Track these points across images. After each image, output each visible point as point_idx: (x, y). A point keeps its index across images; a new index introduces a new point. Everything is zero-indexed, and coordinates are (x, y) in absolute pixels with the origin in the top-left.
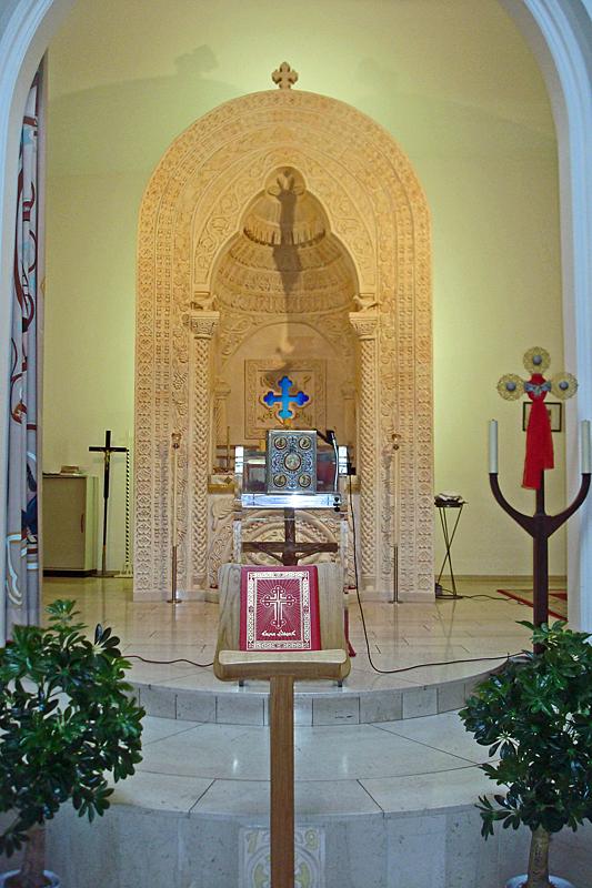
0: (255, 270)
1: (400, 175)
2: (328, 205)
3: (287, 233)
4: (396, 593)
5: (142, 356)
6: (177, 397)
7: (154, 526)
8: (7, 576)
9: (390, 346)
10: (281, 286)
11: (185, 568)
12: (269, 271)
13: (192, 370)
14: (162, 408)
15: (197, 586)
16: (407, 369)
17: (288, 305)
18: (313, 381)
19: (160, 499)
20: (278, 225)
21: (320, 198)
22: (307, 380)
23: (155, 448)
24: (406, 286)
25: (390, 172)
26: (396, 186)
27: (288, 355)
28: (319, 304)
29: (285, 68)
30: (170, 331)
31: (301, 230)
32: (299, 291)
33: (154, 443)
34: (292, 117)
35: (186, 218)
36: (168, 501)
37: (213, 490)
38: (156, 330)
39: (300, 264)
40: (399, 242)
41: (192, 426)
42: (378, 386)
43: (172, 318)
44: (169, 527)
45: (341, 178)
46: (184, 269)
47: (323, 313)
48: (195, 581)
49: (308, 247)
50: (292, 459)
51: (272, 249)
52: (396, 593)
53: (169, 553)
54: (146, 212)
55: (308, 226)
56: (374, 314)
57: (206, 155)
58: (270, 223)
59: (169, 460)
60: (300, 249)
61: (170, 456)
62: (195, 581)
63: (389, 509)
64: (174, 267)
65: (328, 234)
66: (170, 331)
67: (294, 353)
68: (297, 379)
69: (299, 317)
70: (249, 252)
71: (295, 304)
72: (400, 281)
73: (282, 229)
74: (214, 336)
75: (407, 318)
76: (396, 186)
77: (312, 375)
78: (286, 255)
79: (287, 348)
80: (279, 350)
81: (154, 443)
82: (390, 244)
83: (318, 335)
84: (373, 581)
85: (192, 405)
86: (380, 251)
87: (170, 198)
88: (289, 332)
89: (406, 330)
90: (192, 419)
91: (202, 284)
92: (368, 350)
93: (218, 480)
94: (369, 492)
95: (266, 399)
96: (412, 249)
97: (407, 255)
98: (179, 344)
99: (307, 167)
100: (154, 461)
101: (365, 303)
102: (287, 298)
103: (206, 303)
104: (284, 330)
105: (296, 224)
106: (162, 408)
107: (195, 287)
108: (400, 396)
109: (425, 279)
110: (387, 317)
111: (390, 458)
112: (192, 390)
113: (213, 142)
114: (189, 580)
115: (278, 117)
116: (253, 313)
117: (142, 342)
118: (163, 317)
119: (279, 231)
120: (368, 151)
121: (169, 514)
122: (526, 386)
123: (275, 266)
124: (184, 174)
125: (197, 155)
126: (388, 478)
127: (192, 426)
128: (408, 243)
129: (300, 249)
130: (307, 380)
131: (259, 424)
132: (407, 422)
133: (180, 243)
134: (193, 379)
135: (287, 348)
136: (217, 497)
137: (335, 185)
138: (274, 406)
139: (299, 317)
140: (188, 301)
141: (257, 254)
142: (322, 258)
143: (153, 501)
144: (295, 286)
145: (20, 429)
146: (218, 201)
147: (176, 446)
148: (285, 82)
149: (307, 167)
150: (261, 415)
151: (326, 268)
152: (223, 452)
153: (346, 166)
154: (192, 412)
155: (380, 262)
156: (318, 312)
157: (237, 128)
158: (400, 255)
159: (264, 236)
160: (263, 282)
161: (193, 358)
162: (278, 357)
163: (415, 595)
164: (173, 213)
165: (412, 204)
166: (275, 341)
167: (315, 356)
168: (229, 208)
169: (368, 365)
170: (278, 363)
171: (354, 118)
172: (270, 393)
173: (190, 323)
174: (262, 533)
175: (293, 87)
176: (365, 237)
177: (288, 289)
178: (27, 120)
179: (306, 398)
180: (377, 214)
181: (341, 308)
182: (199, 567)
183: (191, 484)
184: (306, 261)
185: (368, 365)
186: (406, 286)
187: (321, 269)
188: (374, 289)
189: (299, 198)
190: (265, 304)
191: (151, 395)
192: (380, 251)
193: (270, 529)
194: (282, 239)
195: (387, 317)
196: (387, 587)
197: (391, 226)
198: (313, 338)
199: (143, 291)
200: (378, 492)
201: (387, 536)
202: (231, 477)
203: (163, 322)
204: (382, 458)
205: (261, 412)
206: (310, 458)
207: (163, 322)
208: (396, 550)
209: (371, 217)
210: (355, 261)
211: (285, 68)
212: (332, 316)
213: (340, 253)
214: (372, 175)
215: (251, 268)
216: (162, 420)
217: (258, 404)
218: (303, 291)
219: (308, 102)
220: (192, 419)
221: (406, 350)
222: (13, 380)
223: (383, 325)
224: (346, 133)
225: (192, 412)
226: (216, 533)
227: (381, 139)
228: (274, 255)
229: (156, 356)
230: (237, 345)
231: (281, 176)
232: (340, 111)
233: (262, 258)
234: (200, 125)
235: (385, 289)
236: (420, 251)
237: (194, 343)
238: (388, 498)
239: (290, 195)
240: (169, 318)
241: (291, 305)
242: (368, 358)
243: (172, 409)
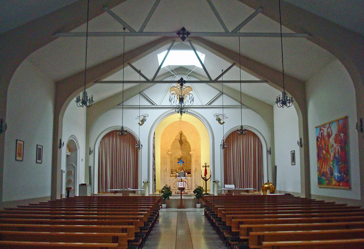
5: (161, 158)
8: (153, 186)
29: (182, 78)
31: (183, 138)
32: (183, 146)
37: (171, 176)
50: (182, 174)
68: (183, 159)
74: (171, 155)
78: (181, 142)
80: (180, 155)
91: (169, 148)
93: (171, 175)
100: (163, 173)
103: (170, 151)
104: (180, 152)
107: (168, 148)
109: (200, 147)
112: (168, 163)
117: (161, 156)
122: (205, 166)
135: (181, 155)
138: (179, 164)
145: (154, 170)
152: (172, 171)
161: (168, 158)
166: (179, 154)
170: (180, 157)
173: (167, 153)
177: (181, 146)
178: (154, 138)
179: (184, 162)
201: (195, 183)
205: (177, 164)
206: (183, 174)
211: (182, 78)
213: (187, 142)
222: (153, 166)
239: (181, 134)
243: (165, 165)
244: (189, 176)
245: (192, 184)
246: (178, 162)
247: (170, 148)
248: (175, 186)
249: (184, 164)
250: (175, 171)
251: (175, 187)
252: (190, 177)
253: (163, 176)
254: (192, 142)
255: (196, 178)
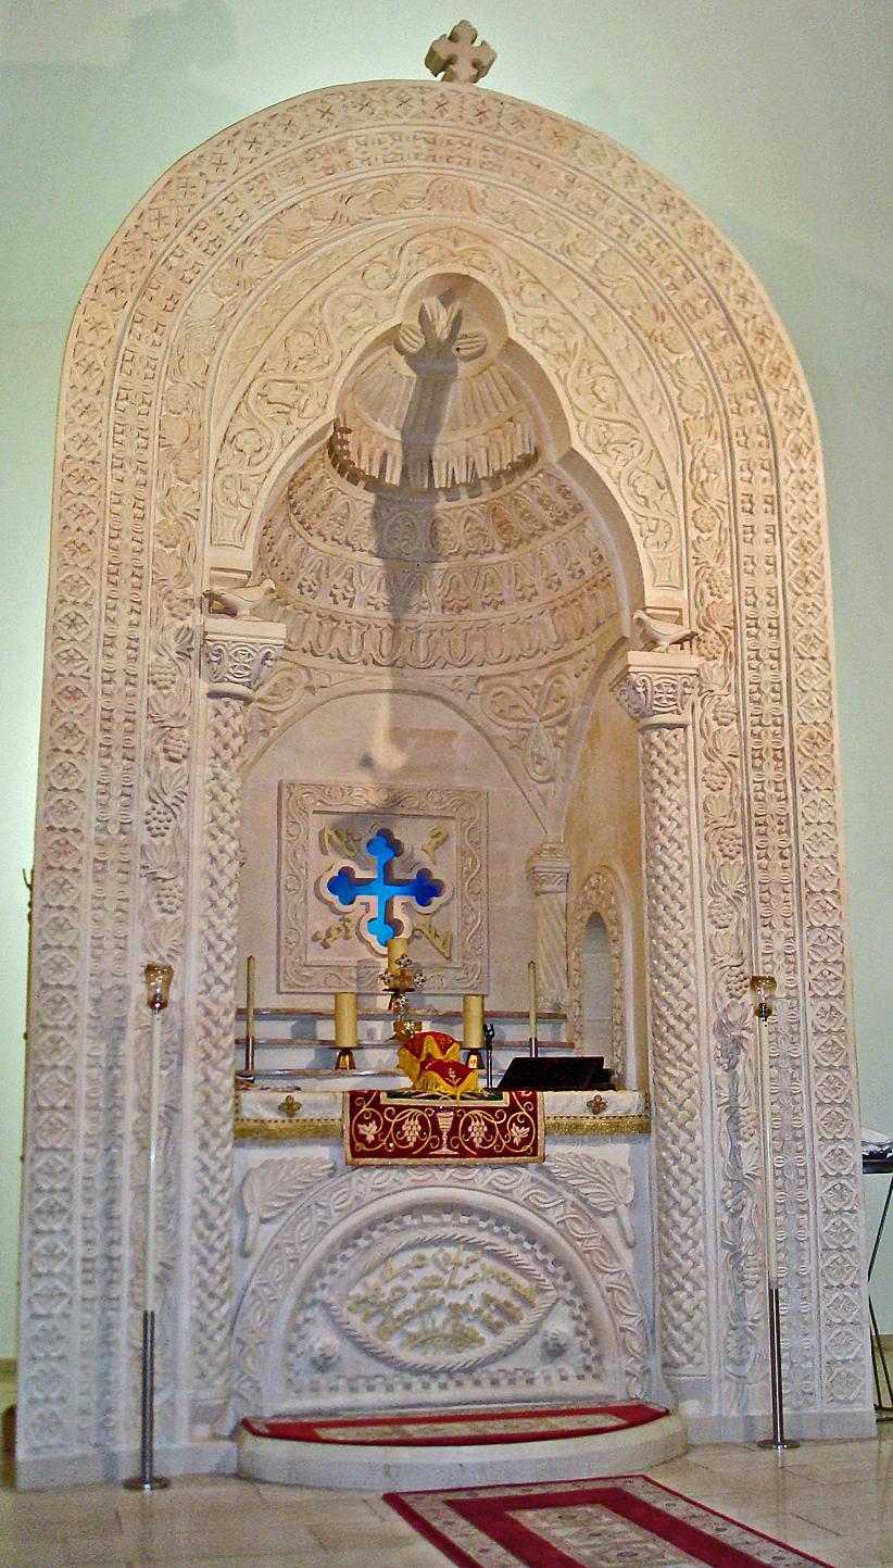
0: (323, 546)
1: (740, 325)
2: (564, 382)
3: (419, 458)
4: (777, 1417)
6: (156, 861)
7: (80, 1249)
9: (727, 744)
10: (382, 597)
11: (172, 1376)
12: (357, 555)
13: (199, 785)
14: (111, 889)
15: (203, 1430)
16: (774, 806)
17: (395, 647)
18: (453, 843)
19: (99, 1167)
20: (398, 437)
21: (542, 361)
22: (441, 839)
23: (89, 1008)
24: (763, 597)
25: (715, 317)
26: (731, 352)
27: (393, 775)
28: (477, 647)
30: (141, 669)
32: (427, 612)
33: (86, 992)
34: (477, 155)
35: (194, 370)
36: (123, 1170)
37: (247, 1134)
38: (102, 663)
39: (435, 545)
40: (741, 487)
41: (195, 944)
42: (698, 851)
43: (146, 635)
44: (125, 1251)
45: (592, 319)
46: (184, 503)
47: (482, 671)
48: (200, 1414)
49: (465, 499)
51: (371, 498)
52: (777, 1417)
53: (127, 1334)
54: (89, 337)
55: (482, 440)
56: (689, 660)
57: (254, 213)
58: (379, 426)
59: (127, 1047)
60: (442, 503)
61: (132, 1033)
62: (200, 1414)
63: (738, 1181)
64: (157, 494)
65: (552, 454)
66: (141, 669)
67: (408, 770)
69: (412, 678)
70: (491, 408)
71: (414, 643)
72: (746, 579)
73: (406, 446)
75: (767, 675)
76: (731, 352)
77: (452, 826)
79: (388, 756)
80: (367, 762)
81: (86, 992)
82: (717, 491)
83: (463, 726)
84: (700, 1389)
85: (198, 884)
86: (692, 506)
87: (153, 310)
88: (396, 716)
89: (768, 707)
90: (197, 924)
92: (668, 752)
94: (684, 1136)
95: (333, 886)
96: (774, 503)
97: (762, 519)
98: (166, 708)
99: (510, 283)
101: (667, 631)
102: (394, 630)
104: (383, 708)
105: (442, 437)
106: (111, 889)
107: (211, 556)
108: (759, 875)
110: (715, 673)
111: (738, 1042)
112: (198, 840)
113: (274, 183)
114: (184, 1413)
115: (442, 151)
116: (309, 660)
118: (122, 629)
119: (398, 451)
120: (662, 259)
121: (125, 1208)
123: (372, 545)
124: (194, 252)
125: (231, 212)
126: (734, 1096)
127: (195, 944)
128: (762, 490)
129: (442, 503)
130: (441, 839)
131: (315, 954)
132: (779, 944)
133: (176, 438)
134: (200, 809)
135: (388, 756)
136: (257, 1155)
137: (580, 335)
139: (422, 679)
140: (195, 591)
141: (340, 500)
142: (504, 527)
143: (80, 1168)
144: (419, 598)
146: (278, 334)
147: (157, 1003)
148: (463, 68)
149: (510, 283)
150: (319, 926)
151: (512, 554)
153: (607, 292)
154: (197, 905)
155: (694, 534)
156: (472, 670)
157: (338, 159)
158: (743, 519)
159: (365, 458)
160: (340, 581)
161: (202, 745)
162: (365, 778)
163: (823, 1420)
164: (159, 352)
165: (771, 397)
167: (459, 781)
168: (310, 357)
169: (670, 791)
170: (365, 794)
171: (630, 178)
172: (345, 873)
173: (199, 652)
174: (385, 1260)
175: (482, 83)
176: (656, 469)
180: (682, 416)
181: (545, 660)
182: (212, 1372)
183: (190, 1120)
184: (455, 535)
185: (670, 791)
186: (763, 597)
187: (494, 558)
188: (681, 598)
189: (463, 368)
190: (339, 640)
191: (82, 847)
192: (692, 506)
193: (409, 1247)
194: (405, 472)
195: (715, 673)
196: (743, 1400)
197: (719, 447)
198: (453, 734)
199: (69, 547)
200: (709, 1133)
202: (297, 1096)
203: (121, 643)
204: (713, 1041)
205: (320, 920)
207: (121, 643)
208: (774, 1297)
209: (666, 421)
210: (634, 529)
212: (516, 682)
214: (670, 322)
215: (316, 541)
216: (110, 924)
217: (312, 899)
218: (435, 612)
219: (518, 122)
220: (197, 924)
221: (769, 758)
223: (706, 693)
224: (608, 212)
225: (197, 905)
226: (252, 1263)
227: (696, 233)
228: (375, 515)
229: (100, 738)
230: (262, 740)
231: (432, 303)
232: (597, 155)
233: (346, 516)
234: (249, 133)
235: (709, 599)
236: (794, 510)
237: (205, 705)
238: (736, 1151)
240: (139, 632)
241: (405, 647)
242: (670, 772)
243: (141, 892)
244: (615, 1129)
245: (666, 1272)
246: (344, 885)
247: (246, 559)
248: (323, 1338)
249: (447, 911)
250: (283, 1030)
251: (323, 1364)
252: (618, 1153)
253: (83, 1125)
254: (664, 485)
255: (748, 1162)
